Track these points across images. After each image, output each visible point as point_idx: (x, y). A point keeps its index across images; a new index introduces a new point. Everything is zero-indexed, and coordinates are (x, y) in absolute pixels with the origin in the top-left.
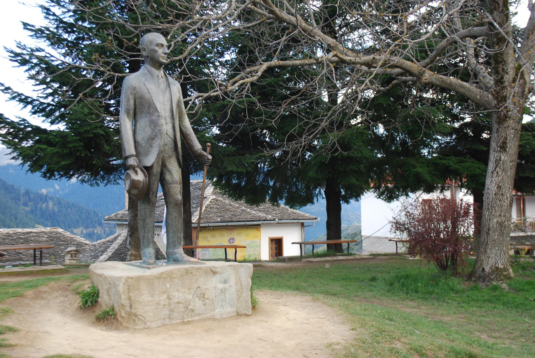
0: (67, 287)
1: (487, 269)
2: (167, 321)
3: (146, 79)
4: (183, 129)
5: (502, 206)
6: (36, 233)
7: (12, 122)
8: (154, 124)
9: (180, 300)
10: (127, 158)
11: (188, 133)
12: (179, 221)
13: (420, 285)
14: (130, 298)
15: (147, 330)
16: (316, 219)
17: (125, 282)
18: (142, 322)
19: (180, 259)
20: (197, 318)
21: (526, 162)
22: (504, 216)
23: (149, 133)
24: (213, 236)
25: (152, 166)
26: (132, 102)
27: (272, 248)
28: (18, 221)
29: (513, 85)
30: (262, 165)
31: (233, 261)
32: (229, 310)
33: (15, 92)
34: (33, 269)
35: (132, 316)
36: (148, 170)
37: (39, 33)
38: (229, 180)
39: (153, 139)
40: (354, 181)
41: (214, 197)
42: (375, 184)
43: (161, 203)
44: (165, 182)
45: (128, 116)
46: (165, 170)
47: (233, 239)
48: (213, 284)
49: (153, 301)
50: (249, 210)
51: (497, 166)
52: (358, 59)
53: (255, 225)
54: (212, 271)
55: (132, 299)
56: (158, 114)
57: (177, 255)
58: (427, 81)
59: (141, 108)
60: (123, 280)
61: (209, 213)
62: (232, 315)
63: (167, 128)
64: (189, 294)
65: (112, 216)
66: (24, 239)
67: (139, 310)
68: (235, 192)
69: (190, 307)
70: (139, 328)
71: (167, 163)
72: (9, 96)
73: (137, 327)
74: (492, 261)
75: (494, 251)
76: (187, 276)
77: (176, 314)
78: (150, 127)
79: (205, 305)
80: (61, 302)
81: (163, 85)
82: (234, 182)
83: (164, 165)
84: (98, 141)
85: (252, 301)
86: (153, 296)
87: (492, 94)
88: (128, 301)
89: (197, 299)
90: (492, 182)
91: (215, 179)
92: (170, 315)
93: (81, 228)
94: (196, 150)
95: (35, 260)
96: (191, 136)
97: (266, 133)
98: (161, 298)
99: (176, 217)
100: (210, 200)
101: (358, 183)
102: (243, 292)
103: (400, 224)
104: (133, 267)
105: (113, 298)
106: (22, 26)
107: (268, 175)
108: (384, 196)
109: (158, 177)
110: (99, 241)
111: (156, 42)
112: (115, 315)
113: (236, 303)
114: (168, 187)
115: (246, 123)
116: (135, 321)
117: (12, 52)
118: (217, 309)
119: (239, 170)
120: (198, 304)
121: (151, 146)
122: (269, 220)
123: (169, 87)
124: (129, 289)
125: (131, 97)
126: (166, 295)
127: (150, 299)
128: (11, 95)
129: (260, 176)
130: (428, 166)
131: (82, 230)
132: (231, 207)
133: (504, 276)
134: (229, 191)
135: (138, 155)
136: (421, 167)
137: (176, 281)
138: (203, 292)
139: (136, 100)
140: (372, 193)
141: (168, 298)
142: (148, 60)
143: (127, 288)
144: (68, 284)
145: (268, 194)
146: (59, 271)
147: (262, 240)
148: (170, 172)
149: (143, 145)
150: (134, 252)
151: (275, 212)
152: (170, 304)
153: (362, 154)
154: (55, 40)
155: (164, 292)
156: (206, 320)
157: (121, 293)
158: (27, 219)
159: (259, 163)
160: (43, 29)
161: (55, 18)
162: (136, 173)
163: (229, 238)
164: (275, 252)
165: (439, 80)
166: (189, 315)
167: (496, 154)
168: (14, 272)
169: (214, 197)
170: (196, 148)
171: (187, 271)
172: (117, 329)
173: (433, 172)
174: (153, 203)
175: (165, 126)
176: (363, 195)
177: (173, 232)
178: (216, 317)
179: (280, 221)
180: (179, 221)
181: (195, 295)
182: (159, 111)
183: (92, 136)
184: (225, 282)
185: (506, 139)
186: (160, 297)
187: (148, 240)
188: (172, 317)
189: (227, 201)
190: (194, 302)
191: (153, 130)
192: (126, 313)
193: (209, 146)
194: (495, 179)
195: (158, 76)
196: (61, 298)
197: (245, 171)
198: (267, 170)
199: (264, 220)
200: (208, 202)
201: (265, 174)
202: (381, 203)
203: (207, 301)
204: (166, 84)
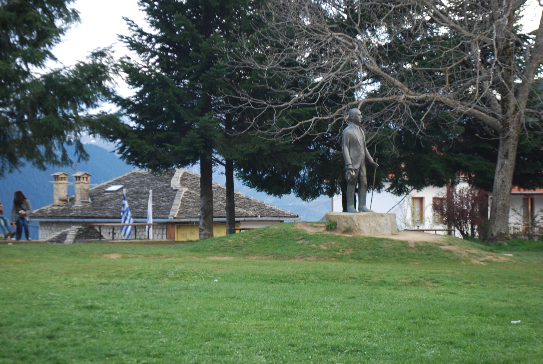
1: (495, 234)
5: (504, 193)
16: (297, 216)
21: (528, 160)
22: (506, 200)
26: (349, 140)
29: (513, 116)
51: (502, 168)
59: (353, 143)
63: (363, 152)
74: (497, 229)
75: (499, 223)
87: (500, 121)
90: (498, 178)
100: (183, 193)
112: (352, 230)
122: (251, 217)
133: (505, 238)
150: (207, 232)
154: (139, 48)
167: (502, 160)
179: (263, 218)
184: (386, 220)
185: (508, 150)
194: (501, 176)
199: (246, 217)
200: (182, 196)
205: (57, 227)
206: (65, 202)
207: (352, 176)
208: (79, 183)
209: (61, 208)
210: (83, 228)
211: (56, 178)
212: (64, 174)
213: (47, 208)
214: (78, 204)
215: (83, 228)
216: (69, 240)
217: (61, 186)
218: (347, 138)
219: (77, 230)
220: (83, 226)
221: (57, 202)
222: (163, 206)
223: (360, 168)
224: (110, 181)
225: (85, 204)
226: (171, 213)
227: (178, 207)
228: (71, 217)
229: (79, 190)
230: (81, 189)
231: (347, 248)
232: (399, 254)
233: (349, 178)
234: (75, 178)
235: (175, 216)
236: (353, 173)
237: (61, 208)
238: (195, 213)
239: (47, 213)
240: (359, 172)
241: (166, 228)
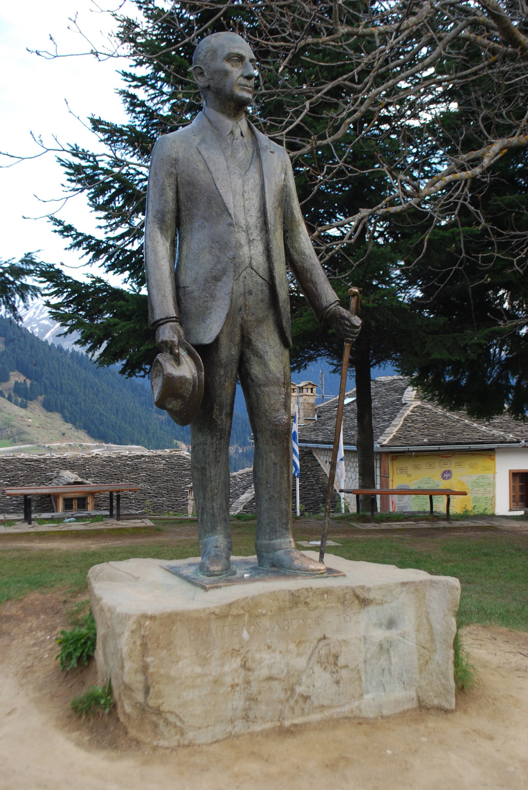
0: (61, 606)
2: (239, 727)
3: (203, 140)
4: (296, 257)
6: (149, 457)
7: (76, 282)
8: (222, 245)
9: (275, 672)
10: (158, 324)
12: (282, 473)
14: (145, 669)
15: (186, 751)
17: (134, 627)
18: (173, 731)
24: (416, 467)
25: (217, 340)
26: (170, 194)
27: (514, 487)
28: (150, 435)
30: (497, 350)
31: (444, 519)
32: (398, 695)
33: (81, 234)
34: (102, 527)
35: (151, 714)
36: (206, 353)
37: (112, 133)
38: (439, 375)
39: (217, 279)
41: (419, 403)
44: (249, 381)
45: (161, 229)
46: (248, 353)
47: (449, 472)
48: (360, 630)
49: (205, 675)
50: (475, 425)
53: (486, 451)
54: (357, 597)
55: (151, 670)
56: (229, 220)
60: (131, 622)
61: (409, 429)
62: (406, 707)
64: (298, 655)
66: (131, 465)
67: (169, 700)
68: (450, 397)
69: (299, 690)
70: (166, 744)
71: (254, 337)
72: (70, 241)
76: (295, 610)
77: (263, 707)
78: (210, 253)
79: (338, 682)
80: (34, 645)
81: (243, 153)
82: (447, 379)
83: (246, 342)
85: (456, 673)
86: (204, 661)
88: (140, 677)
89: (317, 669)
91: (415, 374)
92: (247, 710)
93: (236, 446)
94: (325, 304)
95: (111, 512)
96: (314, 272)
97: (504, 294)
98: (227, 668)
99: (275, 464)
100: (411, 408)
102: (435, 651)
104: (174, 581)
106: (90, 126)
107: (508, 366)
109: (234, 368)
110: (241, 472)
111: (227, 52)
113: (417, 676)
114: (257, 394)
115: (460, 265)
116: (156, 726)
118: (367, 692)
119: (453, 358)
120: (319, 682)
121: (213, 297)
122: (510, 442)
123: (259, 156)
124: (144, 645)
126: (239, 660)
127: (198, 670)
128: (75, 239)
129: (493, 369)
131: (237, 448)
132: (446, 420)
134: (440, 395)
135: (182, 316)
137: (265, 622)
138: (333, 651)
139: (180, 189)
141: (243, 666)
142: (210, 95)
143: (139, 642)
144: (63, 598)
145: (508, 399)
146: (144, 531)
147: (497, 476)
149: (196, 294)
151: (519, 428)
152: (248, 683)
155: (235, 653)
156: (335, 723)
157: (125, 655)
158: (162, 432)
159: (491, 347)
160: (125, 129)
161: (145, 109)
162: (177, 360)
163: (443, 470)
164: (519, 494)
166: (297, 710)
168: (72, 531)
169: (419, 403)
170: (324, 298)
171: (295, 599)
172: (113, 745)
174: (221, 430)
175: (246, 249)
177: (270, 499)
178: (364, 714)
180: (282, 473)
181: (315, 659)
182: (231, 211)
184: (391, 624)
186: (222, 665)
187: (213, 515)
188: (251, 715)
189: (440, 410)
190: (309, 676)
191: (218, 257)
192: (135, 705)
193: (355, 294)
195: (232, 133)
196: (39, 634)
197: (463, 360)
198: (506, 359)
200: (408, 412)
201: (501, 365)
203: (344, 673)
204: (250, 150)
225: (309, 422)
235: (384, 443)
238: (420, 437)
241: (380, 460)
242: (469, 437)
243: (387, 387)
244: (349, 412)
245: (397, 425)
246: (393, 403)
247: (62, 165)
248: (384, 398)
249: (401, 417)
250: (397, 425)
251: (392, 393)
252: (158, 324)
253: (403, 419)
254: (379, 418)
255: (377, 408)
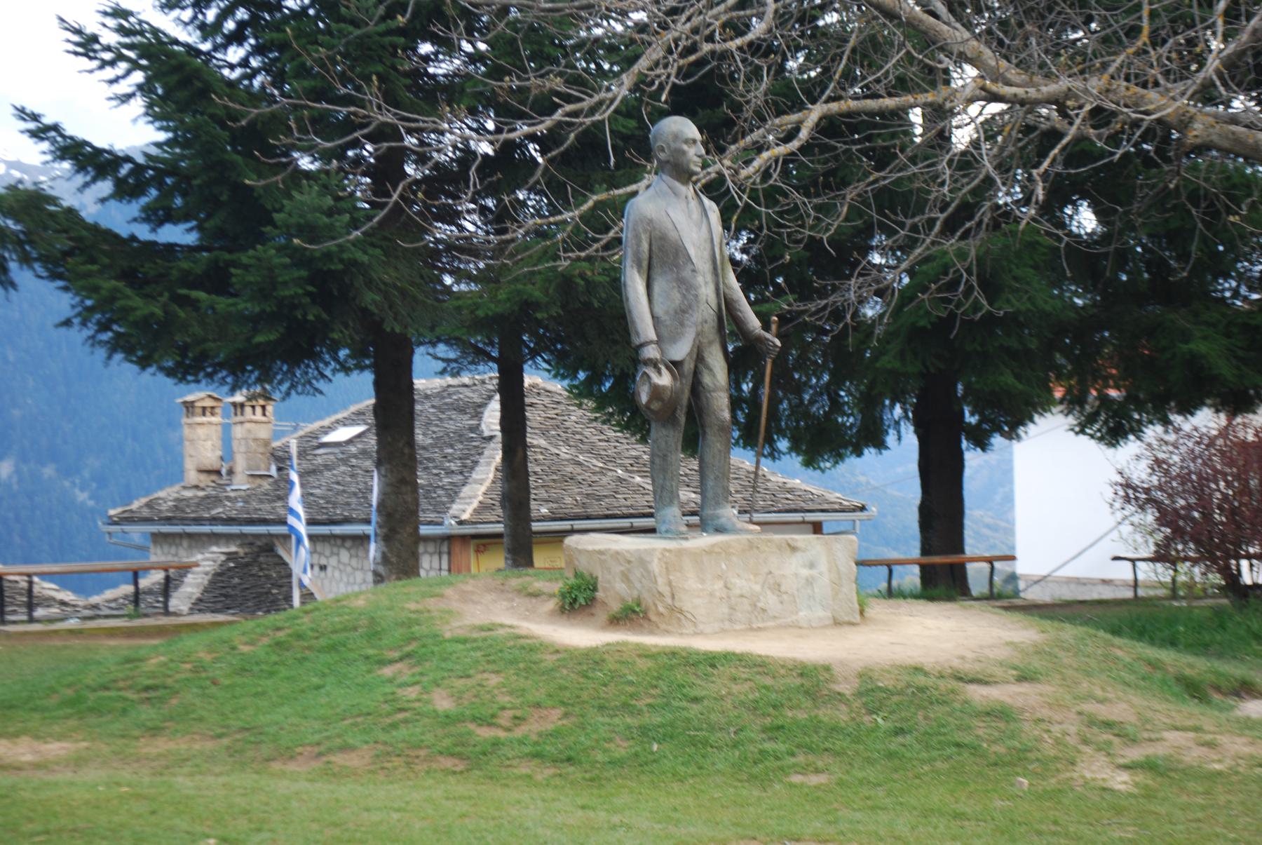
2: (727, 625)
8: (686, 286)
10: (642, 345)
11: (735, 297)
13: (1182, 629)
14: (670, 583)
16: (863, 508)
19: (729, 526)
20: (771, 624)
23: (677, 302)
26: (645, 246)
32: (820, 613)
39: (684, 312)
40: (1008, 379)
42: (1069, 391)
43: (319, 460)
45: (639, 272)
46: (701, 367)
48: (792, 568)
52: (1032, 91)
54: (789, 545)
57: (723, 520)
58: (1198, 141)
59: (664, 256)
63: (707, 292)
65: (135, 505)
67: (686, 604)
69: (760, 605)
71: (706, 355)
73: (684, 631)
81: (696, 214)
84: (347, 280)
88: (668, 588)
89: (769, 592)
92: (730, 615)
101: (1020, 387)
103: (1135, 489)
105: (638, 585)
108: (1096, 426)
112: (645, 613)
114: (707, 398)
117: (78, 32)
121: (682, 324)
125: (643, 237)
130: (1228, 335)
132: (579, 470)
135: (659, 342)
136: (1205, 338)
140: (1060, 418)
148: (711, 370)
153: (1033, 304)
155: (719, 577)
162: (659, 372)
165: (1227, 138)
173: (1240, 353)
176: (1033, 422)
183: (340, 267)
184: (812, 565)
202: (1088, 449)
205: (190, 547)
206: (214, 477)
207: (656, 392)
208: (242, 423)
209: (201, 494)
210: (241, 551)
211: (189, 407)
212: (210, 396)
213: (168, 494)
214: (241, 483)
215: (241, 551)
216: (189, 590)
217: (201, 431)
218: (637, 237)
219: (223, 558)
220: (241, 546)
221: (192, 477)
222: (442, 488)
223: (699, 357)
224: (339, 416)
225: (259, 481)
226: (455, 508)
227: (483, 489)
228: (214, 520)
229: (243, 442)
230: (245, 439)
231: (538, 705)
232: (765, 730)
233: (644, 398)
234: (232, 409)
235: (465, 516)
236: (664, 379)
237: (201, 494)
239: (164, 507)
240: (696, 374)
241: (449, 553)
242: (628, 503)
243: (436, 402)
244: (355, 456)
245: (483, 480)
246: (460, 436)
247: (67, 29)
248: (437, 426)
249: (489, 464)
250: (483, 480)
251: (454, 414)
252: (642, 345)
253: (493, 469)
254: (435, 467)
255: (424, 448)
